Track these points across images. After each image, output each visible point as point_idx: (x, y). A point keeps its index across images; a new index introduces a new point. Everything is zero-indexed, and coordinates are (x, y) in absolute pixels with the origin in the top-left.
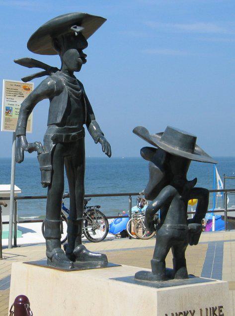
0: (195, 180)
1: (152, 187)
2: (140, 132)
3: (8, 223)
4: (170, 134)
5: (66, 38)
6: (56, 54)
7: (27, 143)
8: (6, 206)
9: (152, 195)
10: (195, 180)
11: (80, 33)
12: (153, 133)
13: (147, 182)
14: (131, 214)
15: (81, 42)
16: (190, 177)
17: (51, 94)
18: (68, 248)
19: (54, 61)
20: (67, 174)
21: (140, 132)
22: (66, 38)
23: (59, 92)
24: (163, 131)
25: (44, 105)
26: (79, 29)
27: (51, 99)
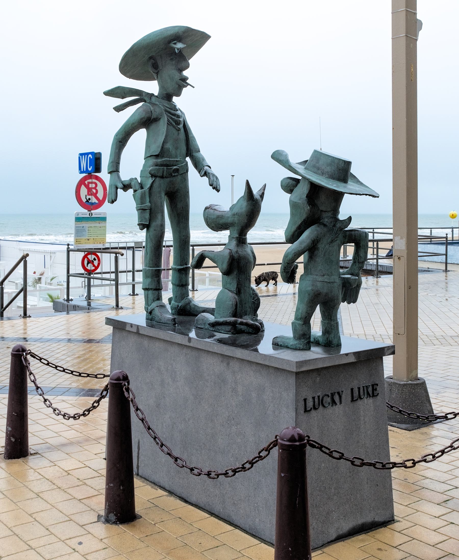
0: (350, 219)
1: (294, 228)
2: (279, 158)
3: (138, 271)
4: (318, 160)
5: (164, 56)
6: (153, 79)
7: (294, 287)
8: (122, 255)
9: (291, 239)
10: (350, 219)
11: (180, 50)
12: (294, 160)
13: (287, 218)
14: (88, 440)
15: (181, 60)
16: (342, 216)
17: (147, 122)
18: (173, 302)
19: (152, 87)
20: (167, 208)
21: (279, 158)
22: (164, 56)
23: (156, 120)
24: (308, 157)
25: (141, 136)
26: (180, 45)
27: (147, 128)
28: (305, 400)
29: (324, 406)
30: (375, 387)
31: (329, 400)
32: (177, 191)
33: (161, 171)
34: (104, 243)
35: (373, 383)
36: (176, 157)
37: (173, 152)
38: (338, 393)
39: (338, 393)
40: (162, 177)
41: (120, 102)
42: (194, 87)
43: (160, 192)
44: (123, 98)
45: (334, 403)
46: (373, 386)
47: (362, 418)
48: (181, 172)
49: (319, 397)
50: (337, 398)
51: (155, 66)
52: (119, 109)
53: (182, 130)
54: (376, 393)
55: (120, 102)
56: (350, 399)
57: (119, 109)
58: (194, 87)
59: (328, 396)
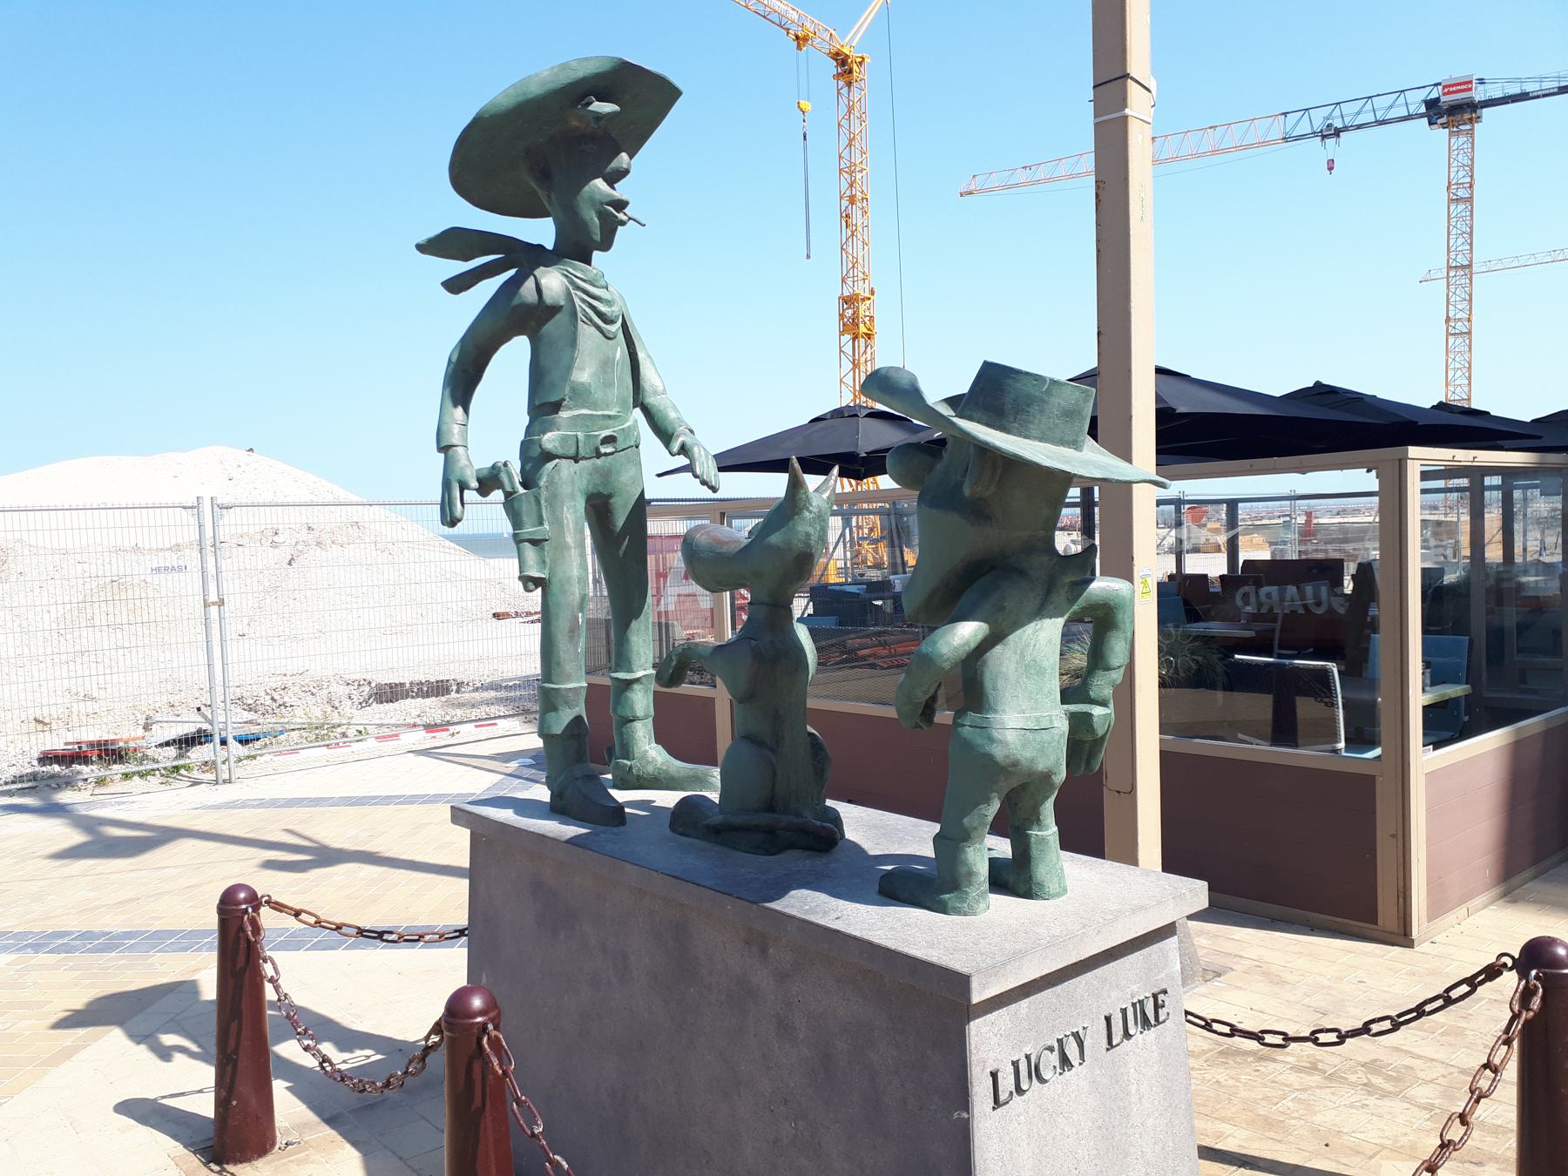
28: (994, 1075)
29: (1042, 1080)
30: (1161, 997)
31: (1054, 1058)
32: (610, 496)
33: (572, 442)
34: (607, 621)
35: (1156, 990)
36: (607, 407)
37: (598, 395)
38: (1076, 1035)
39: (1076, 1035)
40: (576, 459)
41: (458, 267)
42: (659, 475)
43: (573, 496)
44: (466, 260)
45: (1065, 1062)
46: (1155, 996)
47: (1133, 1088)
48: (620, 444)
49: (1028, 1057)
50: (1072, 1050)
51: (544, 175)
52: (456, 285)
53: (621, 335)
54: (1162, 1014)
55: (458, 267)
56: (1105, 1044)
57: (456, 285)
58: (659, 475)
59: (1051, 1049)
